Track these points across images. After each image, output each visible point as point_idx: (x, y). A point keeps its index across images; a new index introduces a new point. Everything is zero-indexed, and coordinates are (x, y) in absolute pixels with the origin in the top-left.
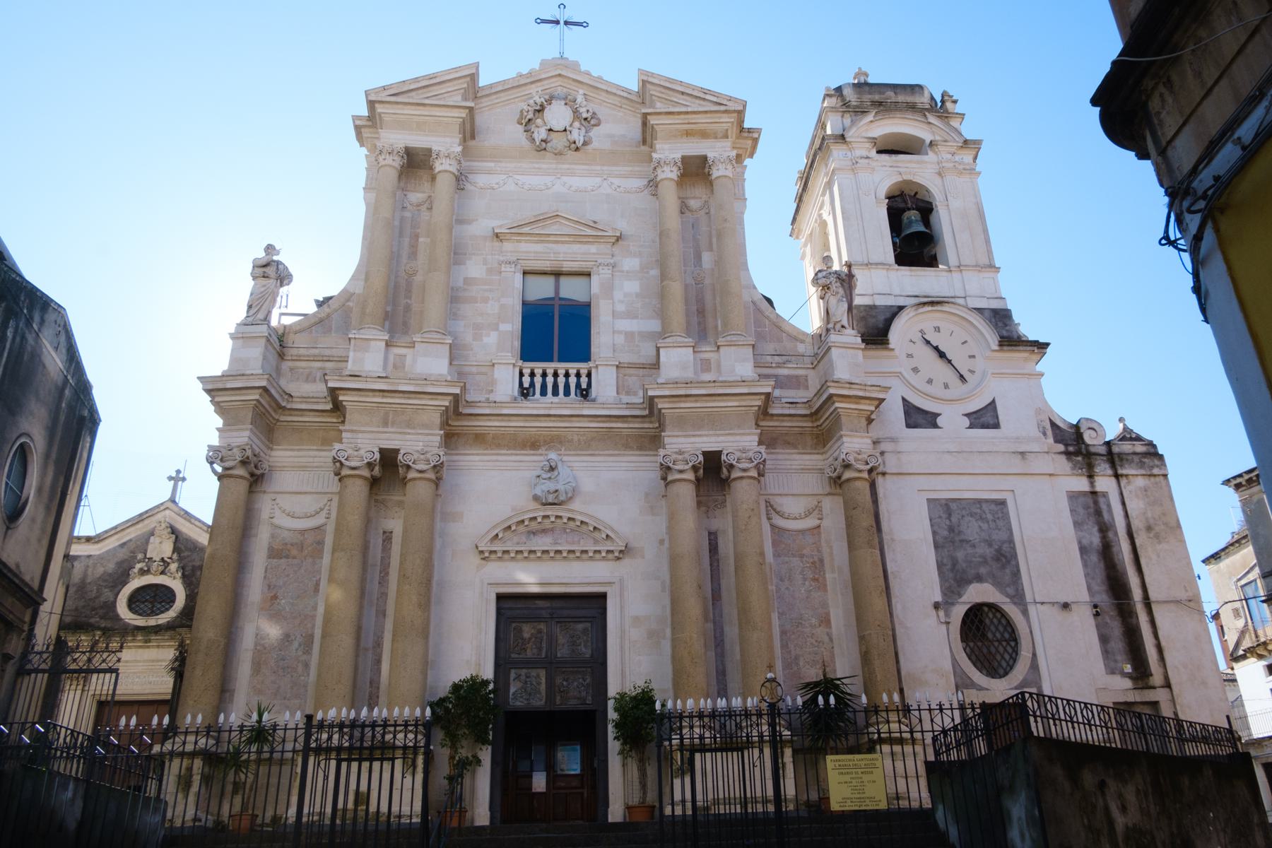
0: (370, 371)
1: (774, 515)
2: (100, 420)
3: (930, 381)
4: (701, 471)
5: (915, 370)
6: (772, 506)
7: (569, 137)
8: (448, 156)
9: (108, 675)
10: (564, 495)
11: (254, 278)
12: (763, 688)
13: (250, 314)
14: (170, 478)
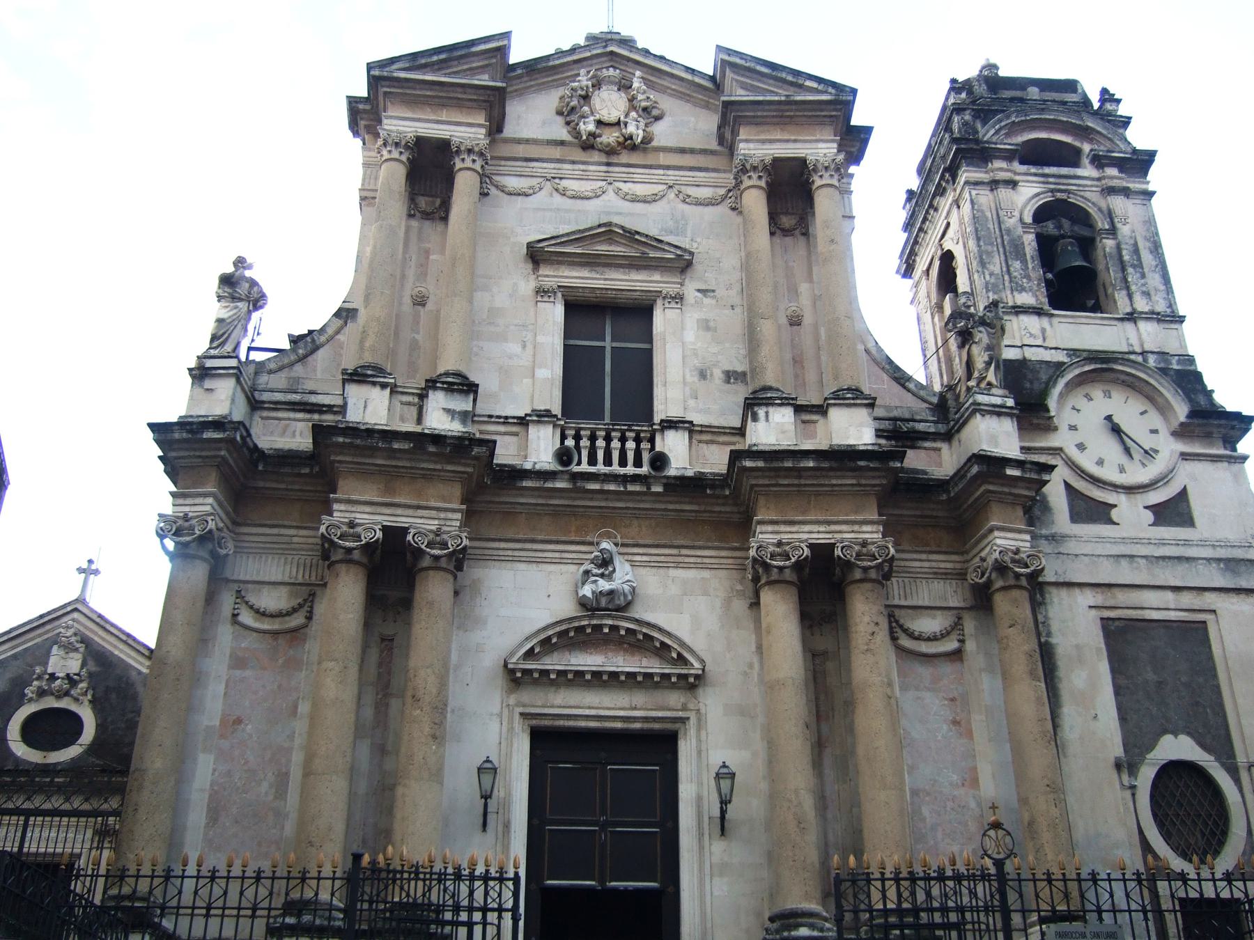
0: (375, 424)
1: (900, 633)
2: (9, 483)
3: (1100, 462)
4: (807, 570)
5: (1081, 447)
6: (897, 622)
7: (624, 131)
8: (470, 151)
9: (14, 818)
10: (622, 598)
11: (220, 298)
12: (1011, 847)
13: (214, 345)
14: (81, 570)
